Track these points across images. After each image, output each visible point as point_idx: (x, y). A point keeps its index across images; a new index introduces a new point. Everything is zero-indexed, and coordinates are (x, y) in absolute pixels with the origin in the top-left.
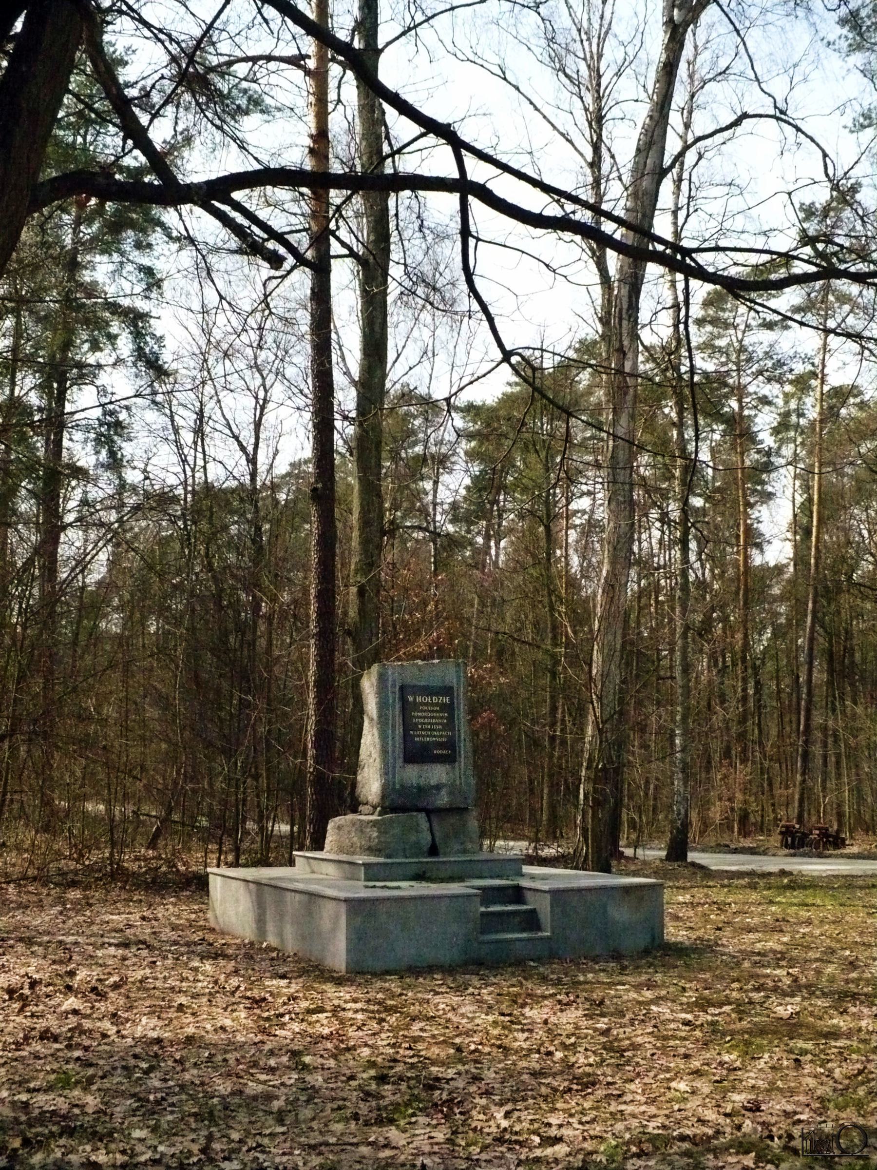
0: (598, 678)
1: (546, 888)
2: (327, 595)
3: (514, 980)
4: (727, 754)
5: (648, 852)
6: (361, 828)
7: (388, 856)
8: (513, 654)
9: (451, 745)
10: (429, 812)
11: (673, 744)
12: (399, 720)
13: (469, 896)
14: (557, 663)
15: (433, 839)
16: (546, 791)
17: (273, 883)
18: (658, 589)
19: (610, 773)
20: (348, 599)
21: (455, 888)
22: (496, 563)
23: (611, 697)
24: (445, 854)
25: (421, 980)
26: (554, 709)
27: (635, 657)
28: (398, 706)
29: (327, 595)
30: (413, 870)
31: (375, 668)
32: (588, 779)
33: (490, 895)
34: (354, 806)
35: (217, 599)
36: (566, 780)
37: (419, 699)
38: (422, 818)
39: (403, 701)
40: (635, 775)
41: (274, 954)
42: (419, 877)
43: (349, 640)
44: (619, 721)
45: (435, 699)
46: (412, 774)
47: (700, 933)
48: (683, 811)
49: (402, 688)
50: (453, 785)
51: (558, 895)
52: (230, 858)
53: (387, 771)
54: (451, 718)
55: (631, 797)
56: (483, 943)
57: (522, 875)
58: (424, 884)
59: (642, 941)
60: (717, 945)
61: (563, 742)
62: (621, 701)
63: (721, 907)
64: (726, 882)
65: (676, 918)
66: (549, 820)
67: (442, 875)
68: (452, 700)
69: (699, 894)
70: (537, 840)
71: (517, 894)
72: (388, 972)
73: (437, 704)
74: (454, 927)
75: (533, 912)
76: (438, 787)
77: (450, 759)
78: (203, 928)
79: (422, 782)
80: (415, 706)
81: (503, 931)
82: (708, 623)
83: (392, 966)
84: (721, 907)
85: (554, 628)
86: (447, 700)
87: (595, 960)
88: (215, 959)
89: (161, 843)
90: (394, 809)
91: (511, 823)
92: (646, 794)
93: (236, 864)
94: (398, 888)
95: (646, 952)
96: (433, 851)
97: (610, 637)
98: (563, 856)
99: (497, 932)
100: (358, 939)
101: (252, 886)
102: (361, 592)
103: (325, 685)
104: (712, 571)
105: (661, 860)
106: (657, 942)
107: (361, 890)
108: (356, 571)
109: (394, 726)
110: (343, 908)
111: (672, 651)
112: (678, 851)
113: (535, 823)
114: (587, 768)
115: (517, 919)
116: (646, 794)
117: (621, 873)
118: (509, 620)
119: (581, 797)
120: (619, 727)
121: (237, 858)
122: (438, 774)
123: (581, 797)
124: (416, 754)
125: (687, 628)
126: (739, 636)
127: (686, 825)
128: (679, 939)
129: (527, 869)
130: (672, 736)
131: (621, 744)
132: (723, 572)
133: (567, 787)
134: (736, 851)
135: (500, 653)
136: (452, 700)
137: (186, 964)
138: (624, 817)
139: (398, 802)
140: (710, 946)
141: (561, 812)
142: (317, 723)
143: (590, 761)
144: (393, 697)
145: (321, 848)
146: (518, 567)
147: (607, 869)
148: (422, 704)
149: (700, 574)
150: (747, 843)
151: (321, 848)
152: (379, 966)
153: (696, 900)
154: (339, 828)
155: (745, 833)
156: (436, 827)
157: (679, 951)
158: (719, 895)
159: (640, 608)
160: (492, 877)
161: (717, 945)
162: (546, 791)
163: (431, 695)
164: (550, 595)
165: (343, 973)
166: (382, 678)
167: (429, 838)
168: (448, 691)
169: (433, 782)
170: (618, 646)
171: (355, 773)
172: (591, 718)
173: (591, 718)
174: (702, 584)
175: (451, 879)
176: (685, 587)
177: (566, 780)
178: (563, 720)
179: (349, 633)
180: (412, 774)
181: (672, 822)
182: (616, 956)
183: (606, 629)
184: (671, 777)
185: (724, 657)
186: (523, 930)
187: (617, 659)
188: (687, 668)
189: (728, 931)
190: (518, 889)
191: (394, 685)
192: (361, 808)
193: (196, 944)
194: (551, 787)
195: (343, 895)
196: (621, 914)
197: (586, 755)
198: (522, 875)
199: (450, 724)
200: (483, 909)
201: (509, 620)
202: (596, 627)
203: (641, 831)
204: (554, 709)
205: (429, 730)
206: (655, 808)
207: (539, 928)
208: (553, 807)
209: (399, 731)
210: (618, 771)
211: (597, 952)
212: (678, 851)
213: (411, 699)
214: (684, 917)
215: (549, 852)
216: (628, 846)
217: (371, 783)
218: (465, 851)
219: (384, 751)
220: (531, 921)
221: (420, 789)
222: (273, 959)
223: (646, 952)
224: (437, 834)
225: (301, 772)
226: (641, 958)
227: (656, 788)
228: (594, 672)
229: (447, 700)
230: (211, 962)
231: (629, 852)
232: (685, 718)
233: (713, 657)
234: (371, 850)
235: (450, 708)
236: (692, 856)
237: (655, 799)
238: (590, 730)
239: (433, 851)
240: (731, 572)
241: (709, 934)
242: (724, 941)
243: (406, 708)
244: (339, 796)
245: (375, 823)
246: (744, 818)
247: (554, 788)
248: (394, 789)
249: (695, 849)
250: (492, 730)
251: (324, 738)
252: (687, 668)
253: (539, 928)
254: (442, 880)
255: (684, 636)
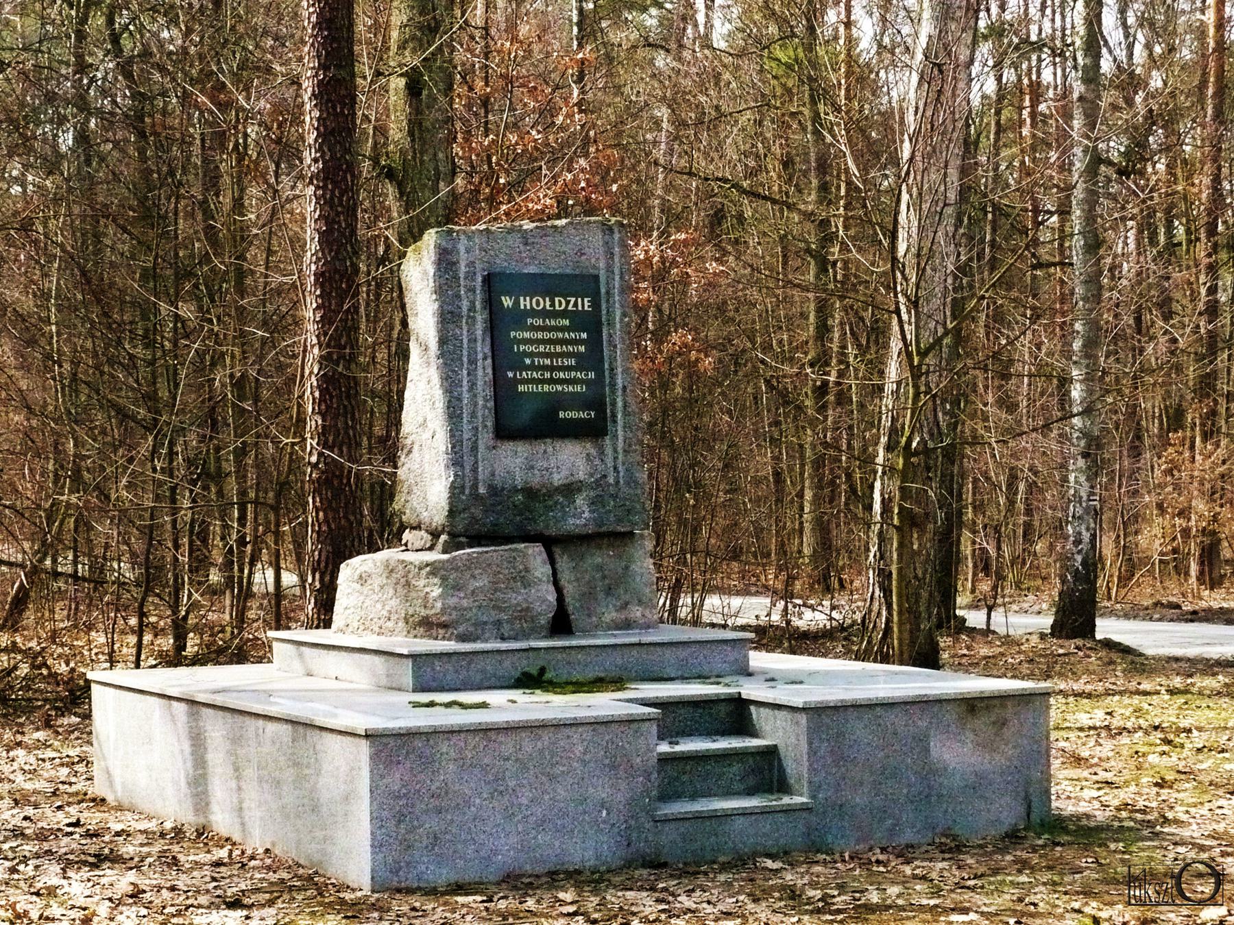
0: (910, 261)
1: (798, 702)
2: (337, 93)
3: (728, 904)
4: (1176, 419)
5: (1014, 619)
6: (403, 580)
7: (462, 638)
8: (740, 218)
9: (597, 401)
10: (550, 544)
11: (1064, 399)
12: (483, 348)
13: (630, 721)
14: (828, 238)
15: (560, 598)
16: (808, 495)
17: (219, 700)
18: (1037, 91)
19: (937, 463)
20: (386, 107)
21: (604, 704)
22: (707, 43)
23: (936, 302)
24: (586, 632)
25: (530, 903)
26: (823, 330)
27: (991, 229)
28: (481, 318)
29: (337, 93)
30: (511, 667)
31: (430, 237)
32: (889, 470)
33: (677, 717)
34: (387, 530)
35: (136, 120)
36: (849, 476)
37: (525, 303)
38: (535, 555)
39: (490, 307)
40: (989, 460)
41: (223, 853)
42: (530, 681)
43: (390, 190)
44: (955, 355)
45: (560, 303)
46: (513, 462)
47: (1125, 795)
48: (1086, 536)
49: (488, 280)
50: (601, 482)
51: (823, 717)
52: (167, 643)
53: (460, 454)
54: (595, 343)
55: (979, 508)
56: (667, 820)
57: (749, 674)
58: (540, 696)
59: (1004, 811)
60: (1166, 821)
61: (843, 398)
62: (958, 308)
63: (1170, 738)
64: (1177, 682)
65: (1078, 761)
66: (814, 556)
67: (577, 676)
68: (596, 304)
69: (1123, 709)
70: (788, 595)
71: (736, 715)
72: (460, 888)
73: (564, 314)
74: (600, 790)
75: (771, 752)
76: (570, 490)
77: (593, 432)
78: (82, 798)
79: (535, 480)
80: (519, 318)
81: (709, 794)
82: (1137, 155)
83: (470, 876)
84: (1170, 738)
85: (823, 167)
86: (586, 304)
87: (906, 853)
88: (94, 866)
89: (30, 617)
90: (476, 539)
91: (739, 561)
92: (1011, 502)
93: (175, 659)
94: (484, 705)
95: (1013, 838)
96: (561, 624)
97: (934, 176)
98: (842, 628)
99: (694, 797)
100: (396, 818)
101: (180, 708)
102: (414, 88)
103: (337, 281)
104: (1148, 46)
105: (1043, 636)
106: (1035, 817)
107: (402, 712)
108: (402, 47)
109: (473, 362)
110: (364, 749)
111: (1064, 211)
112: (1075, 618)
113: (787, 564)
114: (889, 448)
115: (736, 768)
116: (1011, 502)
117: (966, 666)
118: (731, 153)
119: (877, 507)
120: (958, 359)
121: (180, 646)
122: (568, 460)
123: (877, 507)
124: (521, 419)
125: (1097, 160)
126: (1203, 181)
127: (1092, 564)
128: (1083, 808)
129: (759, 659)
130: (1065, 382)
131: (958, 398)
132: (1172, 49)
133: (853, 489)
134: (1194, 617)
135: (718, 217)
136: (596, 304)
137: (30, 881)
138: (967, 549)
139: (485, 520)
140: (1150, 824)
141: (839, 536)
142: (323, 360)
143: (894, 432)
144: (472, 300)
145: (327, 624)
146: (753, 46)
147: (928, 658)
148: (533, 313)
149: (1122, 54)
150: (1215, 599)
151: (327, 624)
152: (443, 876)
153: (1116, 722)
154: (362, 579)
155: (1212, 580)
156: (566, 577)
157: (1085, 833)
158: (1164, 710)
159: (1000, 129)
160: (684, 679)
161: (1166, 821)
162: (808, 495)
163: (551, 293)
164: (814, 102)
165: (367, 891)
166: (445, 261)
167: (552, 597)
168: (587, 284)
169: (558, 479)
170: (952, 196)
171: (393, 460)
172: (896, 345)
173: (896, 345)
174: (1129, 82)
175: (597, 684)
176: (1092, 76)
177: (849, 476)
178: (843, 355)
179: (390, 174)
180: (513, 462)
181: (1065, 558)
182: (953, 848)
183: (927, 157)
184: (1063, 466)
185: (1169, 227)
186: (750, 792)
187: (948, 224)
188: (1095, 245)
189: (1185, 793)
190: (740, 705)
191: (471, 276)
192: (407, 535)
193: (56, 832)
194: (819, 486)
195: (362, 723)
196: (956, 754)
197: (886, 422)
198: (749, 674)
199: (593, 358)
200: (664, 748)
201: (731, 153)
202: (906, 154)
203: (1001, 577)
204: (823, 330)
205: (547, 372)
206: (1028, 527)
207: (783, 787)
208: (823, 529)
209: (484, 372)
210: (951, 454)
211: (908, 836)
212: (1075, 618)
213: (507, 302)
214: (1095, 758)
215: (811, 619)
216: (974, 606)
217: (426, 479)
218: (627, 625)
219: (453, 413)
220: (766, 771)
221: (530, 493)
222: (218, 864)
223: (1013, 838)
224: (569, 589)
225: (296, 463)
226: (1004, 851)
227: (1031, 486)
228: (902, 248)
229: (586, 304)
230: (85, 873)
231: (975, 619)
232: (1091, 344)
233: (1147, 228)
234: (428, 625)
235: (592, 323)
236: (1106, 628)
237: (1029, 512)
238: (893, 370)
239: (561, 624)
240: (1186, 54)
241: (1143, 794)
242: (1179, 813)
243: (499, 324)
244: (359, 515)
245: (434, 569)
246: (1209, 554)
247: (826, 491)
248: (475, 496)
249: (1112, 613)
250: (692, 369)
251: (340, 391)
252: (1095, 245)
253: (783, 787)
254: (579, 687)
255: (1091, 171)
